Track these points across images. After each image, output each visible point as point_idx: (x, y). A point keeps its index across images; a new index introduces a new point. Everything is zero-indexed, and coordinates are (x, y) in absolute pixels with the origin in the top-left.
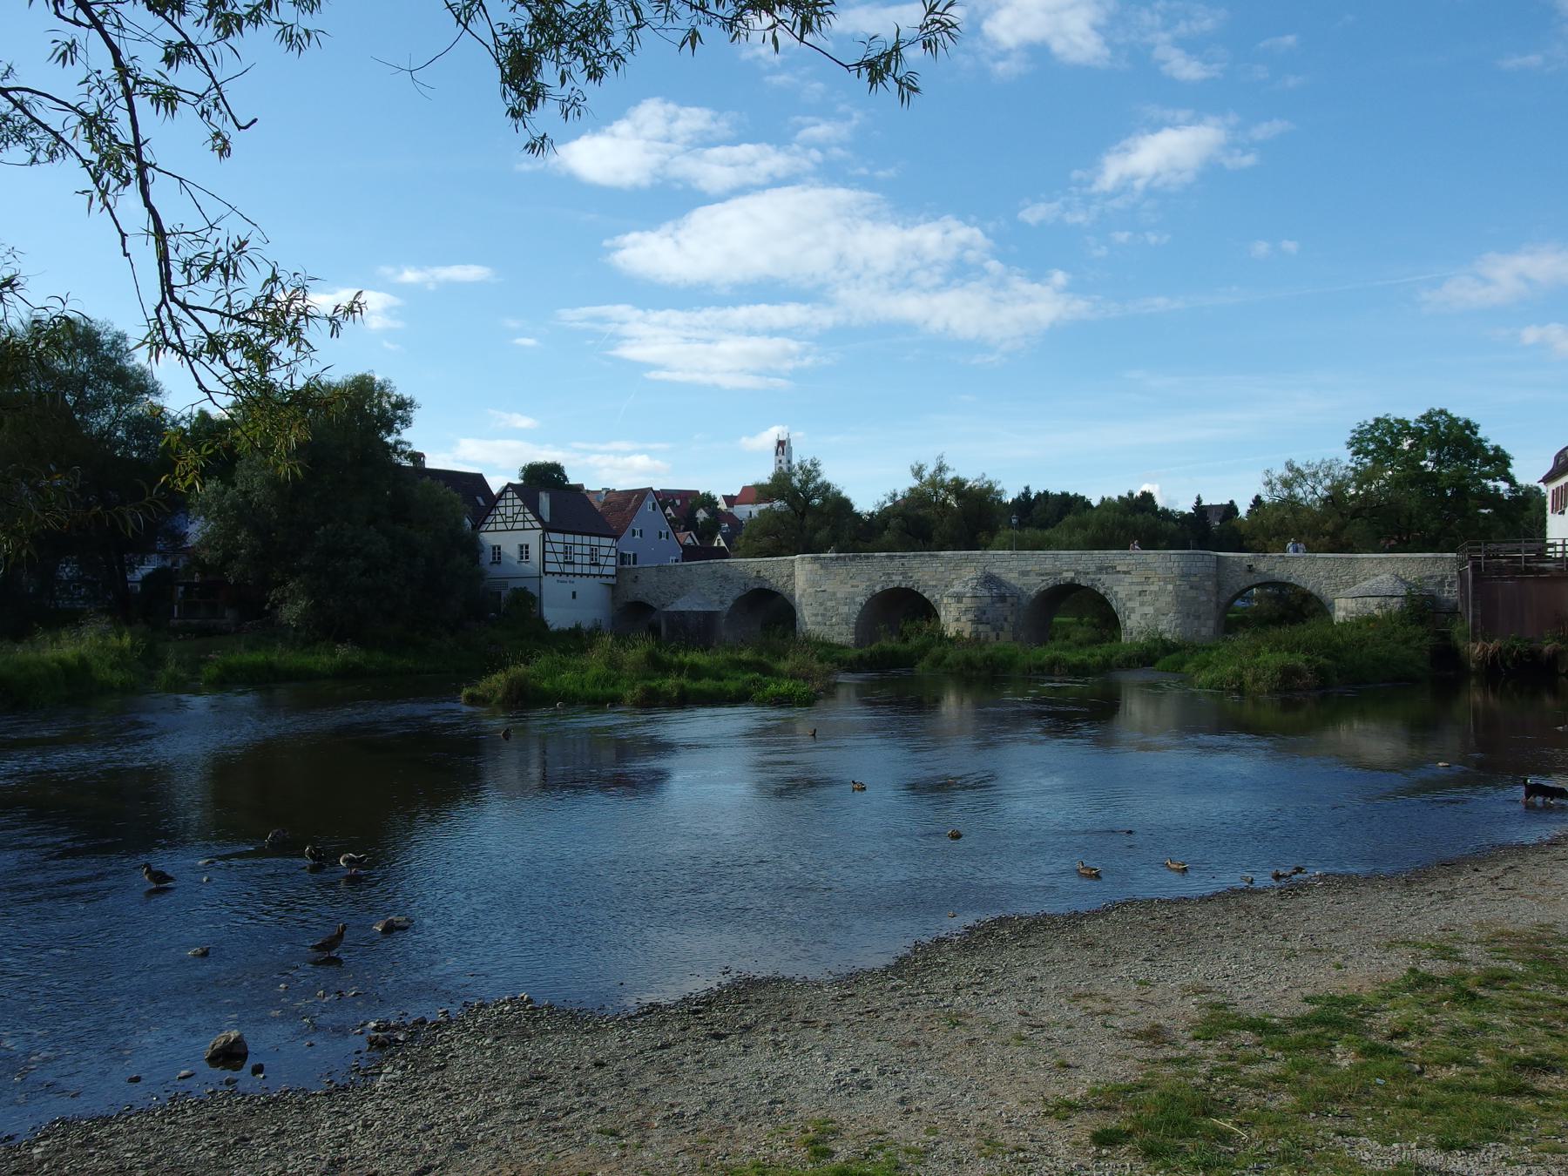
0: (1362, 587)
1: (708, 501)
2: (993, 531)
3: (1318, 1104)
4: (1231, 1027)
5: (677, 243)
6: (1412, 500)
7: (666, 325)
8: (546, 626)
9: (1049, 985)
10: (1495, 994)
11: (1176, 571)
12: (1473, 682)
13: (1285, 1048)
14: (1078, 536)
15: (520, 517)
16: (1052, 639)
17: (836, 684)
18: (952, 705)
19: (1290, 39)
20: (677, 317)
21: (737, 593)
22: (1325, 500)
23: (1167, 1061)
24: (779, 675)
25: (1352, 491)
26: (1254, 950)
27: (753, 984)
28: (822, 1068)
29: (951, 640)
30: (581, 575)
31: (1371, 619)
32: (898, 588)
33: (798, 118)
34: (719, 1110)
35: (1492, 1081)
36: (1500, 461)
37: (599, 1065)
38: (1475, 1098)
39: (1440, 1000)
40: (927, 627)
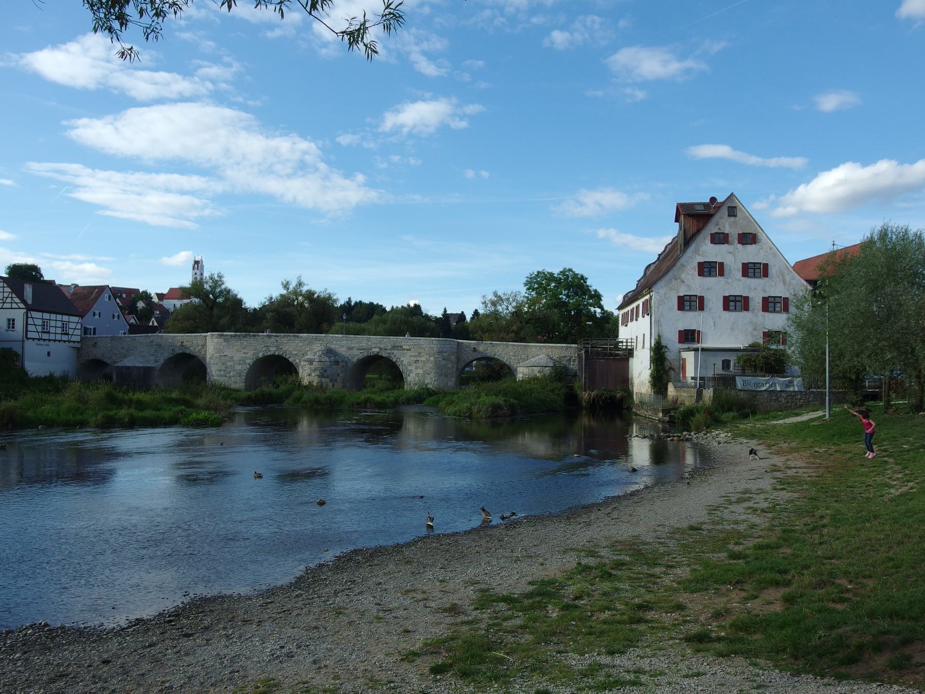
0: (531, 361)
1: (146, 296)
2: (331, 323)
3: (545, 638)
4: (494, 601)
5: (116, 129)
6: (555, 314)
7: (109, 180)
8: (27, 374)
9: (391, 586)
10: (619, 573)
11: (435, 350)
12: (584, 412)
13: (524, 610)
14: (381, 328)
15: (9, 300)
16: (366, 387)
17: (234, 414)
18: (305, 426)
19: (481, 63)
20: (117, 177)
21: (167, 355)
22: (513, 313)
23: (463, 623)
24: (198, 408)
25: (526, 309)
26: (498, 559)
27: (205, 600)
28: (260, 648)
29: (306, 387)
30: (55, 341)
31: (535, 379)
32: (273, 355)
33: (198, 61)
34: (196, 682)
35: (625, 617)
36: (597, 297)
37: (106, 662)
38: (620, 626)
39: (595, 578)
40: (291, 379)
